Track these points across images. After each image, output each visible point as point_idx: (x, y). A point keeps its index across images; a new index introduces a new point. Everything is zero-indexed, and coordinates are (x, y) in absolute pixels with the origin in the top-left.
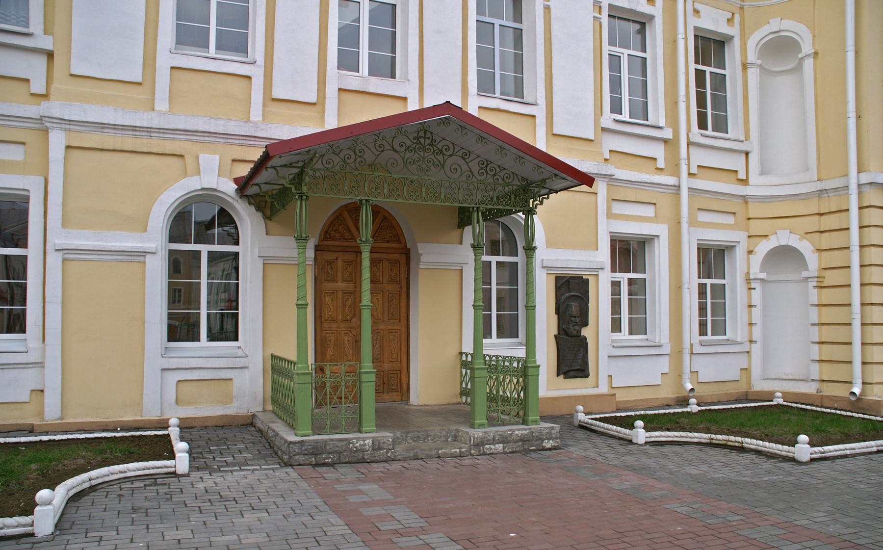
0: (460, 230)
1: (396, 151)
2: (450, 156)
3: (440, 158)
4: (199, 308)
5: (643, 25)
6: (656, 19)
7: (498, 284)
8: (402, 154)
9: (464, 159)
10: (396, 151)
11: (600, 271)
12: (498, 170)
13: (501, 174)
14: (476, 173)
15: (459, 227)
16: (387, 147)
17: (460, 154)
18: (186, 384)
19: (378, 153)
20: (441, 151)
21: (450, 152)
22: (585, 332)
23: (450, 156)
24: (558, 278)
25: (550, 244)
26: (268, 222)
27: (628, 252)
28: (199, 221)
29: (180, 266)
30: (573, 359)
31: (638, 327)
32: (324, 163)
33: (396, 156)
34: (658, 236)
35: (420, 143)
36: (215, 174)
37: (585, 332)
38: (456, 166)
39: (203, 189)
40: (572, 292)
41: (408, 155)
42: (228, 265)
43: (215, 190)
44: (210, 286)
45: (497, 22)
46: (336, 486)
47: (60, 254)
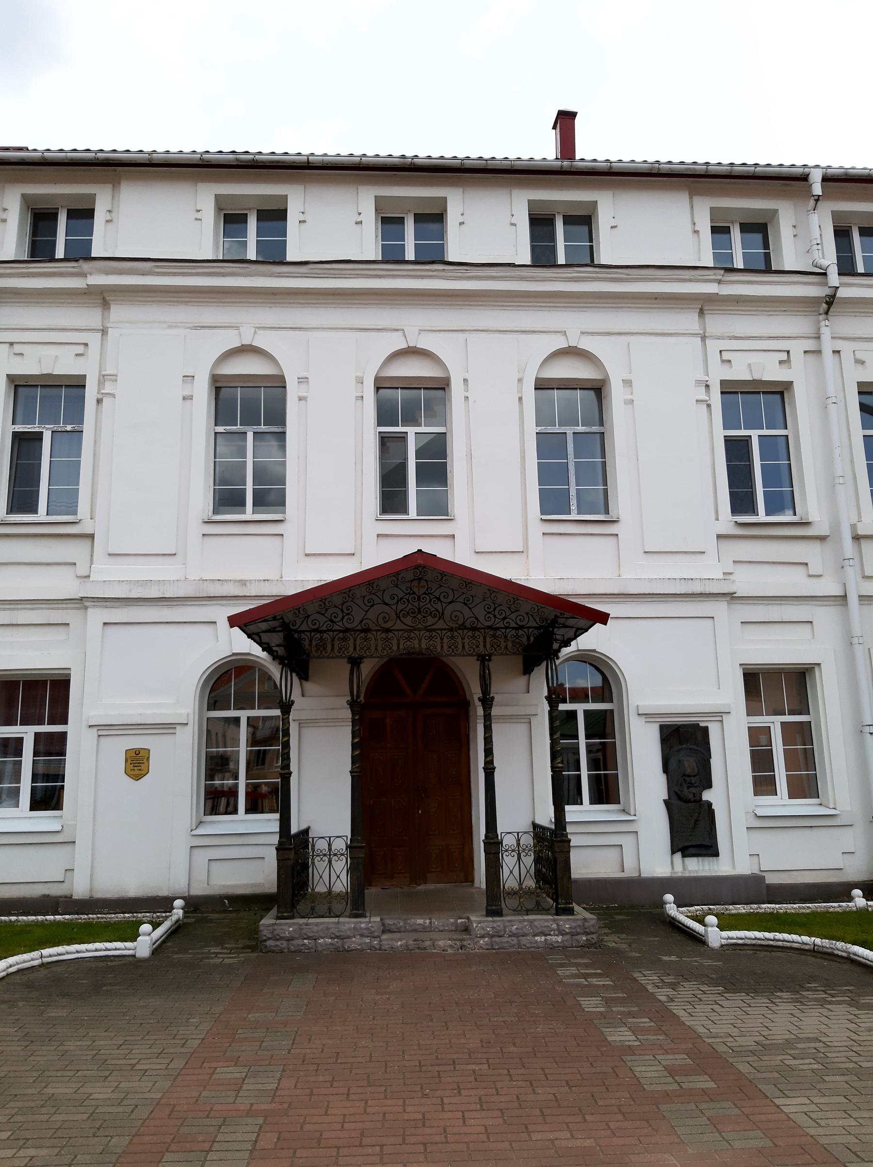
0: (526, 677)
1: (387, 604)
2: (450, 603)
3: (439, 606)
4: (242, 771)
5: (782, 393)
6: (796, 386)
7: (587, 737)
8: (394, 607)
9: (466, 604)
10: (387, 604)
11: (724, 716)
12: (508, 612)
13: (513, 616)
14: (482, 619)
15: (524, 674)
16: (377, 600)
17: (461, 599)
18: (218, 863)
19: (366, 608)
20: (439, 599)
21: (450, 599)
22: (707, 796)
23: (450, 603)
24: (663, 728)
25: (37, 735)
26: (304, 683)
27: (779, 687)
29: (216, 735)
30: (693, 827)
31: (805, 786)
32: (310, 623)
33: (387, 609)
34: (819, 664)
35: (414, 593)
37: (707, 796)
38: (458, 613)
39: (234, 654)
40: (686, 746)
41: (401, 606)
43: (248, 654)
44: (588, 746)
45: (569, 431)
46: (712, 1085)
47: (95, 730)
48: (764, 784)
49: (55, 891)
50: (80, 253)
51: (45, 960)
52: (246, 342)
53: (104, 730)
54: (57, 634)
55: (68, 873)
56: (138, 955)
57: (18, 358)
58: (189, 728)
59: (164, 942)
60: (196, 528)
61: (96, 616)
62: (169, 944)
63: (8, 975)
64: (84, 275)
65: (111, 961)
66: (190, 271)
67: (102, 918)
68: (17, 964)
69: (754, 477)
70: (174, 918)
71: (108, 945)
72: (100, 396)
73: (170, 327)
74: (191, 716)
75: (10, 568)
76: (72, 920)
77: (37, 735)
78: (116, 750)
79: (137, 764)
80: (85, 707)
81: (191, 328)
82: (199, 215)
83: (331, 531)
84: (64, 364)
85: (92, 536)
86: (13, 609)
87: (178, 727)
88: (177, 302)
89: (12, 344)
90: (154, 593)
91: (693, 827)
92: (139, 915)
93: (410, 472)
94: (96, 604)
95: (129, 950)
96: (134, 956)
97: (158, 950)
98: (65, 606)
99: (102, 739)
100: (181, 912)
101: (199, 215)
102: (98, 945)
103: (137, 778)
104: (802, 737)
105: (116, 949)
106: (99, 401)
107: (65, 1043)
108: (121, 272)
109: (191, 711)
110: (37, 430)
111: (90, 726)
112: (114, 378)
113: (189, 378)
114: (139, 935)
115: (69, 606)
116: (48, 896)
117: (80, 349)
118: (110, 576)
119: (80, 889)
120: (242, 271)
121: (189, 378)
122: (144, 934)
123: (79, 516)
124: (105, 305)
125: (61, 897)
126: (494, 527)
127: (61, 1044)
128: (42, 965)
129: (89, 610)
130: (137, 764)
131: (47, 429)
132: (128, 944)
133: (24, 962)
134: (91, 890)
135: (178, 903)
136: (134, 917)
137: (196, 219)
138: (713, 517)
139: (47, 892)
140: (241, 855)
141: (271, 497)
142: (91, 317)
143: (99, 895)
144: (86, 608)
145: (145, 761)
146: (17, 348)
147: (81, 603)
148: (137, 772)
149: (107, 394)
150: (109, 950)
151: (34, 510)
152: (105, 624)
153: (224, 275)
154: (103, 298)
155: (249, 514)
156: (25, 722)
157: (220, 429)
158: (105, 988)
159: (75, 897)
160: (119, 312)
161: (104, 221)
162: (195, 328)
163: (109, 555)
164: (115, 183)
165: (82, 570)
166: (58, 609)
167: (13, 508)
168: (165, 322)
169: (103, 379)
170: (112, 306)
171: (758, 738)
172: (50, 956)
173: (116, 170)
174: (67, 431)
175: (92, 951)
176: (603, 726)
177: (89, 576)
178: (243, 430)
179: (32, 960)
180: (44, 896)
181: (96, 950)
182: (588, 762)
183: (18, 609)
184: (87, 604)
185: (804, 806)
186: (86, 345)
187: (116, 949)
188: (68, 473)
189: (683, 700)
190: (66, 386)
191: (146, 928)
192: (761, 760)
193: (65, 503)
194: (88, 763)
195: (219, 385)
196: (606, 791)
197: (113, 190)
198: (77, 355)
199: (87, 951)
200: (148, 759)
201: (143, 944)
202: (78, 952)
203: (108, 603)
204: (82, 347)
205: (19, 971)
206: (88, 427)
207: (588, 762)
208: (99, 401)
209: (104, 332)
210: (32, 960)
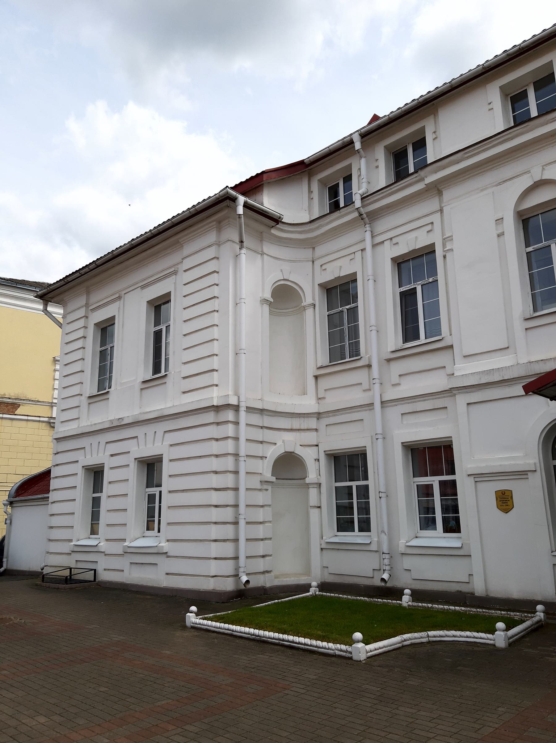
25: (441, 482)
47: (472, 477)
49: (464, 588)
50: (422, 165)
51: (431, 639)
52: (537, 178)
53: (479, 477)
54: (441, 415)
55: (471, 577)
56: (497, 645)
57: (396, 246)
58: (538, 473)
59: (523, 637)
60: (519, 326)
61: (462, 400)
62: (527, 639)
63: (403, 646)
64: (422, 179)
65: (478, 647)
66: (488, 146)
67: (486, 612)
68: (410, 639)
70: (536, 619)
71: (476, 634)
72: (444, 253)
73: (482, 190)
74: (538, 465)
75: (407, 376)
76: (466, 611)
77: (441, 482)
78: (489, 490)
79: (505, 501)
80: (466, 462)
81: (497, 185)
82: (491, 106)
84: (419, 240)
85: (451, 347)
86: (413, 402)
87: (529, 473)
88: (484, 171)
89: (391, 239)
90: (497, 378)
92: (512, 613)
94: (460, 391)
95: (491, 640)
96: (495, 645)
97: (514, 644)
98: (442, 396)
99: (478, 484)
100: (542, 615)
101: (491, 106)
102: (468, 633)
103: (507, 511)
105: (481, 638)
106: (445, 257)
107: (400, 708)
108: (444, 168)
109: (537, 461)
110: (413, 287)
111: (469, 475)
112: (450, 238)
113: (500, 221)
114: (496, 631)
115: (445, 395)
116: (461, 591)
117: (429, 228)
118: (466, 370)
119: (479, 588)
120: (525, 129)
121: (500, 221)
122: (500, 630)
123: (443, 336)
124: (440, 193)
125: (468, 593)
127: (397, 709)
128: (429, 642)
129: (456, 396)
130: (505, 501)
131: (418, 285)
132: (490, 636)
133: (416, 638)
134: (487, 591)
135: (540, 607)
136: (508, 614)
137: (489, 110)
139: (460, 589)
142: (432, 204)
143: (492, 595)
144: (455, 395)
145: (510, 498)
146: (395, 241)
147: (451, 392)
148: (505, 507)
149: (448, 250)
150: (476, 638)
151: (417, 337)
152: (468, 404)
153: (512, 138)
154: (436, 189)
156: (434, 474)
157: (530, 249)
158: (459, 668)
159: (476, 595)
160: (448, 194)
161: (432, 139)
162: (500, 184)
163: (464, 357)
164: (434, 113)
165: (449, 370)
166: (439, 398)
167: (406, 340)
168: (478, 189)
169: (445, 241)
170: (444, 192)
172: (435, 637)
173: (433, 104)
174: (430, 283)
175: (465, 637)
177: (453, 374)
178: (547, 245)
179: (421, 638)
180: (458, 591)
181: (467, 637)
183: (416, 402)
184: (454, 392)
185: (450, 541)
186: (432, 223)
187: (481, 638)
188: (433, 310)
190: (426, 254)
191: (500, 625)
193: (434, 329)
195: (524, 217)
197: (435, 117)
198: (428, 232)
199: (461, 636)
200: (512, 497)
201: (500, 637)
202: (454, 636)
203: (467, 390)
204: (430, 225)
205: (412, 644)
206: (440, 277)
208: (445, 257)
209: (441, 211)
210: (421, 638)
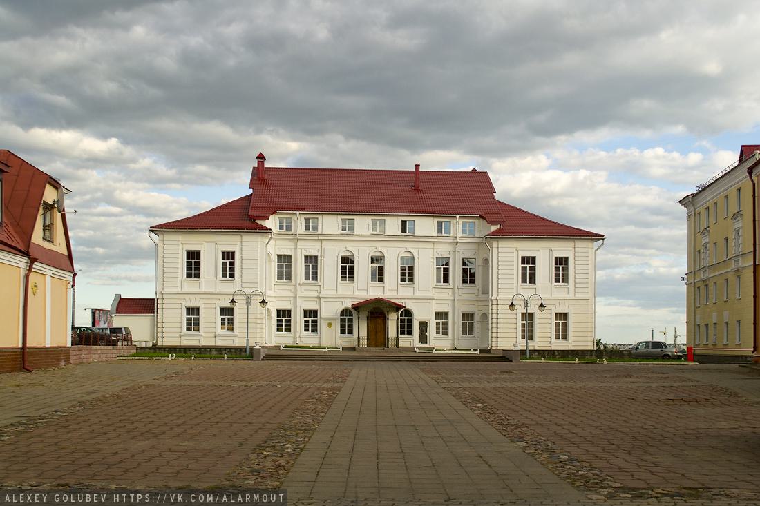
4: (346, 324)
27: (442, 315)
28: (345, 312)
30: (423, 338)
36: (349, 304)
40: (423, 325)
42: (351, 320)
48: (438, 332)
53: (325, 319)
69: (229, 270)
83: (363, 289)
91: (423, 338)
93: (380, 276)
104: (445, 324)
126: (392, 289)
130: (330, 325)
138: (654, 332)
140: (343, 341)
141: (197, 324)
155: (377, 282)
171: (438, 324)
176: (410, 321)
182: (406, 328)
189: (423, 318)
192: (438, 328)
194: (322, 325)
196: (410, 333)
207: (406, 328)
